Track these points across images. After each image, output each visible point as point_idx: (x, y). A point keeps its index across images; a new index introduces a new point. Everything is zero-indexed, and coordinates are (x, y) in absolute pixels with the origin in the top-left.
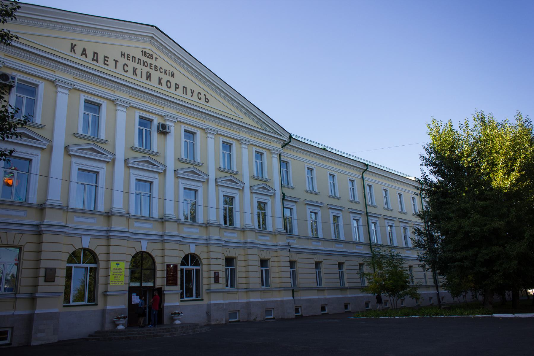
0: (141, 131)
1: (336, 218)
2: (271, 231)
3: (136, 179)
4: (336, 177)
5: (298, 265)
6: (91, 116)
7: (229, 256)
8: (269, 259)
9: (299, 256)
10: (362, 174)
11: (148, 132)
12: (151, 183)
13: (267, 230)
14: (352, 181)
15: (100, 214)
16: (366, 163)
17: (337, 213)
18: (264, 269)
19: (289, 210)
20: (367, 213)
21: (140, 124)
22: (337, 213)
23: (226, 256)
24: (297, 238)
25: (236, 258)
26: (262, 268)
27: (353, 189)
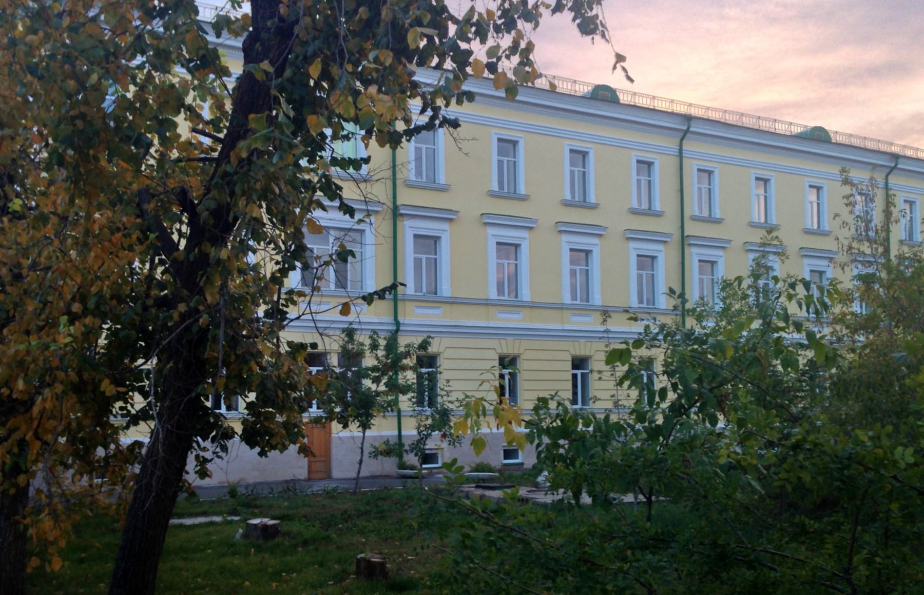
0: (500, 163)
1: (582, 255)
2: (665, 308)
3: (498, 243)
4: (592, 158)
5: (522, 365)
6: (505, 162)
7: (505, 351)
8: (590, 357)
9: (525, 344)
10: (887, 176)
11: (512, 164)
12: (517, 246)
13: (656, 306)
14: (646, 166)
15: (594, 309)
16: (895, 149)
17: (584, 242)
18: (579, 372)
19: (710, 265)
20: (395, 208)
21: (500, 152)
22: (584, 242)
23: (573, 353)
24: (663, 314)
25: (590, 357)
26: (575, 372)
27: (710, 189)
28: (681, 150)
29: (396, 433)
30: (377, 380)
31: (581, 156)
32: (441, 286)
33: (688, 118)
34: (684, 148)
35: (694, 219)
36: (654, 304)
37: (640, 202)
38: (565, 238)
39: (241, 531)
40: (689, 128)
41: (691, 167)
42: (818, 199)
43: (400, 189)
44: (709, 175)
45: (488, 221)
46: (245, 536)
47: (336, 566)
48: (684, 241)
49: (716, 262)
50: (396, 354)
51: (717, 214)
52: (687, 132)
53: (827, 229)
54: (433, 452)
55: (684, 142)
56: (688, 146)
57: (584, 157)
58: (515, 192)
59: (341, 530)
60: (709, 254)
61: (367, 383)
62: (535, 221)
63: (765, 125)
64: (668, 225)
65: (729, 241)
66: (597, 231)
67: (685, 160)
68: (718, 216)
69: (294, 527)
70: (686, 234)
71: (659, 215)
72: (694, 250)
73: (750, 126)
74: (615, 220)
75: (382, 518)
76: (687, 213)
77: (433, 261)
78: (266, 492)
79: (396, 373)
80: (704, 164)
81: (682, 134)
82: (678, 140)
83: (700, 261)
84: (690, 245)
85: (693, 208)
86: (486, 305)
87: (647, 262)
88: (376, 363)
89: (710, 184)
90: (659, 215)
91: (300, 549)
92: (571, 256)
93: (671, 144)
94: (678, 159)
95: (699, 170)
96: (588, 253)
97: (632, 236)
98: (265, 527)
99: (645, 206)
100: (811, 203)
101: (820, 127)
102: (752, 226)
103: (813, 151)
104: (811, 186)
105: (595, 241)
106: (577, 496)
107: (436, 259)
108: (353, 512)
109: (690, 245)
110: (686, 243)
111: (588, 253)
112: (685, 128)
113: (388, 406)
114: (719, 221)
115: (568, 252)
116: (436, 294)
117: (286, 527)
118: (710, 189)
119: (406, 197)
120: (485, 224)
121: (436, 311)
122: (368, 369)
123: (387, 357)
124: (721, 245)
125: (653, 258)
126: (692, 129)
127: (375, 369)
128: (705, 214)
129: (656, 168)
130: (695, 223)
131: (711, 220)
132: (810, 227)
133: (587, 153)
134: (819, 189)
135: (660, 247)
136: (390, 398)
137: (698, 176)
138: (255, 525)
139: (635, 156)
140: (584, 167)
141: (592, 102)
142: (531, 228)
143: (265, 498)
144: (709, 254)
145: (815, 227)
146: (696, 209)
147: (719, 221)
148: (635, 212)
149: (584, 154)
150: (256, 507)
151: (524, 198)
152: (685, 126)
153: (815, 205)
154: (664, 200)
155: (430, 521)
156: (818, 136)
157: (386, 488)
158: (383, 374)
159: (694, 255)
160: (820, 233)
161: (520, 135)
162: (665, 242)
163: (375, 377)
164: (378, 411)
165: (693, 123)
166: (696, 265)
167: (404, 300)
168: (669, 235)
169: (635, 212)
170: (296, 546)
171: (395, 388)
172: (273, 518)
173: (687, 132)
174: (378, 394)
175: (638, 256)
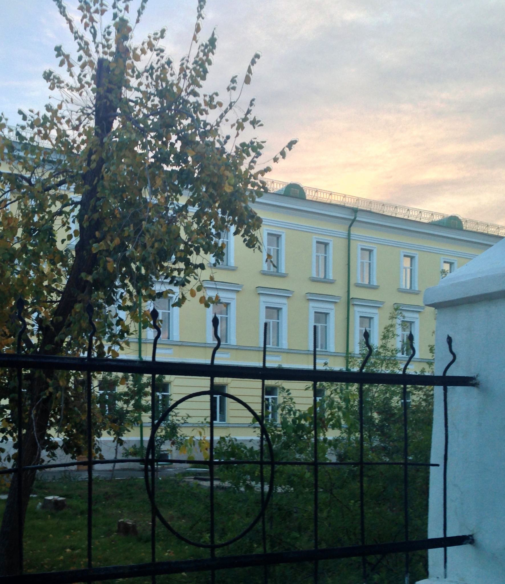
10: (350, 226)
22: (275, 302)
27: (370, 264)
28: (349, 234)
29: (139, 438)
30: (127, 402)
31: (275, 238)
32: (172, 333)
33: (355, 211)
34: (352, 233)
35: (357, 285)
36: (326, 348)
37: (318, 272)
38: (263, 298)
39: (40, 504)
40: (355, 218)
41: (356, 247)
42: (411, 266)
43: (352, 288)
44: (370, 254)
45: (262, 292)
46: (43, 507)
47: (104, 528)
48: (349, 302)
49: (372, 318)
50: (141, 384)
51: (375, 283)
52: (354, 221)
53: (417, 289)
54: (166, 452)
55: (351, 228)
56: (354, 231)
57: (278, 239)
58: (227, 265)
59: (104, 505)
60: (368, 312)
61: (120, 404)
62: (241, 286)
63: (388, 212)
64: (338, 290)
65: (383, 303)
66: (286, 294)
67: (351, 241)
68: (375, 284)
69: (74, 502)
70: (351, 297)
71: (332, 282)
72: (357, 309)
73: (377, 212)
74: (300, 287)
75: (131, 498)
76: (352, 282)
77: (167, 314)
78: (50, 478)
79: (140, 398)
80: (321, 237)
81: (350, 222)
82: (348, 226)
83: (361, 317)
84: (354, 305)
85: (357, 277)
86: (205, 347)
87: (322, 316)
88: (126, 390)
89: (370, 260)
90: (332, 282)
91: (79, 517)
92: (315, 316)
93: (341, 230)
94: (347, 240)
95: (362, 249)
96: (279, 310)
97: (311, 297)
98: (56, 502)
99: (322, 276)
100: (406, 268)
101: (455, 217)
102: (357, 286)
103: (436, 233)
104: (405, 256)
105: (285, 301)
106: (237, 485)
107: (169, 313)
108: (112, 494)
109: (354, 305)
110: (351, 303)
111: (279, 310)
112: (353, 218)
113: (135, 421)
114: (375, 288)
115: (265, 309)
116: (169, 338)
117: (69, 502)
118: (370, 264)
119: (355, 293)
120: (309, 300)
121: (168, 351)
122: (121, 394)
123: (134, 386)
124: (376, 305)
125: (326, 314)
126: (357, 219)
127: (126, 394)
128: (366, 282)
129: (331, 247)
130: (357, 288)
131: (371, 287)
132: (404, 287)
133: (280, 236)
134: (412, 258)
135: (332, 306)
136: (136, 415)
137: (361, 254)
138: (50, 500)
139: (315, 238)
140: (278, 246)
141: (286, 198)
142: (238, 291)
143: (50, 482)
144: (368, 312)
145: (408, 287)
146: (359, 278)
147: (375, 288)
148: (314, 280)
149: (278, 237)
150: (46, 489)
151: (283, 276)
152: (352, 216)
153: (408, 271)
154: (335, 271)
155: (163, 501)
156: (453, 223)
157: (132, 477)
158: (132, 398)
159: (357, 312)
160: (411, 292)
161: (417, 252)
162: (335, 302)
163: (125, 399)
164: (128, 424)
165: (358, 214)
166: (358, 320)
167: (146, 343)
168: (339, 298)
169: (314, 280)
170: (77, 514)
171: (138, 408)
172: (61, 496)
173: (354, 221)
174: (128, 412)
175: (316, 312)
